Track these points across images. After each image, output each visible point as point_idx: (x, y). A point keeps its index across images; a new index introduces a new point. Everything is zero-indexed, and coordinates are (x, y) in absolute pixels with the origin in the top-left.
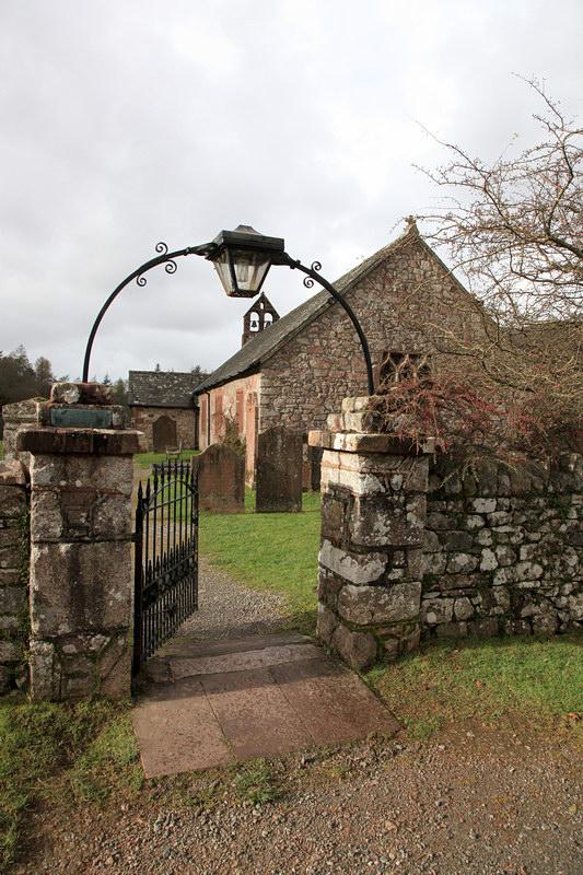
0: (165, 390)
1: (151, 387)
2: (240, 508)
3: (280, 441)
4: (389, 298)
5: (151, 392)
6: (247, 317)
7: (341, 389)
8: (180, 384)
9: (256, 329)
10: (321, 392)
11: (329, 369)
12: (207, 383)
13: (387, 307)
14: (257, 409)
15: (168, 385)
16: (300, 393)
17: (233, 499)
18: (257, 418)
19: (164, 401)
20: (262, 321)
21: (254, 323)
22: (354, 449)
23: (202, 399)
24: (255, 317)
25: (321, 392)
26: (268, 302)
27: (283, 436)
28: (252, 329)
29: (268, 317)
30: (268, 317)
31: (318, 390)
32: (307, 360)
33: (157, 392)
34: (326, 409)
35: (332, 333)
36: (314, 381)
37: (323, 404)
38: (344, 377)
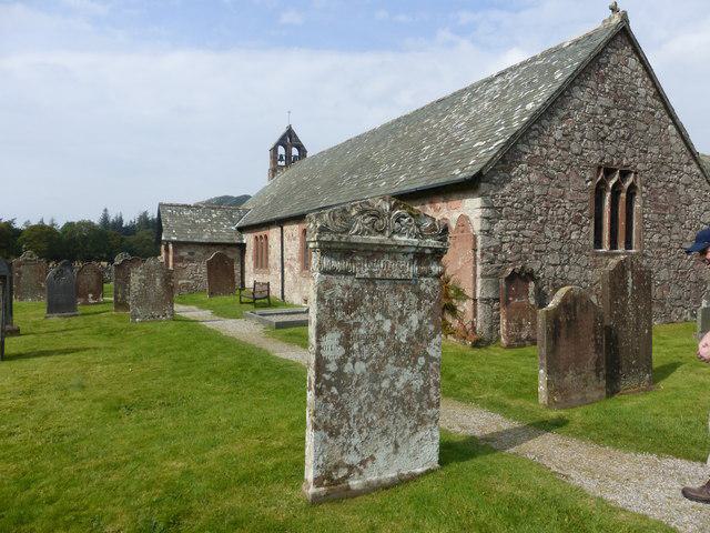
0: (205, 226)
3: (630, 281)
6: (275, 150)
9: (283, 163)
15: (206, 219)
17: (594, 377)
24: (281, 150)
30: (295, 152)
33: (194, 226)
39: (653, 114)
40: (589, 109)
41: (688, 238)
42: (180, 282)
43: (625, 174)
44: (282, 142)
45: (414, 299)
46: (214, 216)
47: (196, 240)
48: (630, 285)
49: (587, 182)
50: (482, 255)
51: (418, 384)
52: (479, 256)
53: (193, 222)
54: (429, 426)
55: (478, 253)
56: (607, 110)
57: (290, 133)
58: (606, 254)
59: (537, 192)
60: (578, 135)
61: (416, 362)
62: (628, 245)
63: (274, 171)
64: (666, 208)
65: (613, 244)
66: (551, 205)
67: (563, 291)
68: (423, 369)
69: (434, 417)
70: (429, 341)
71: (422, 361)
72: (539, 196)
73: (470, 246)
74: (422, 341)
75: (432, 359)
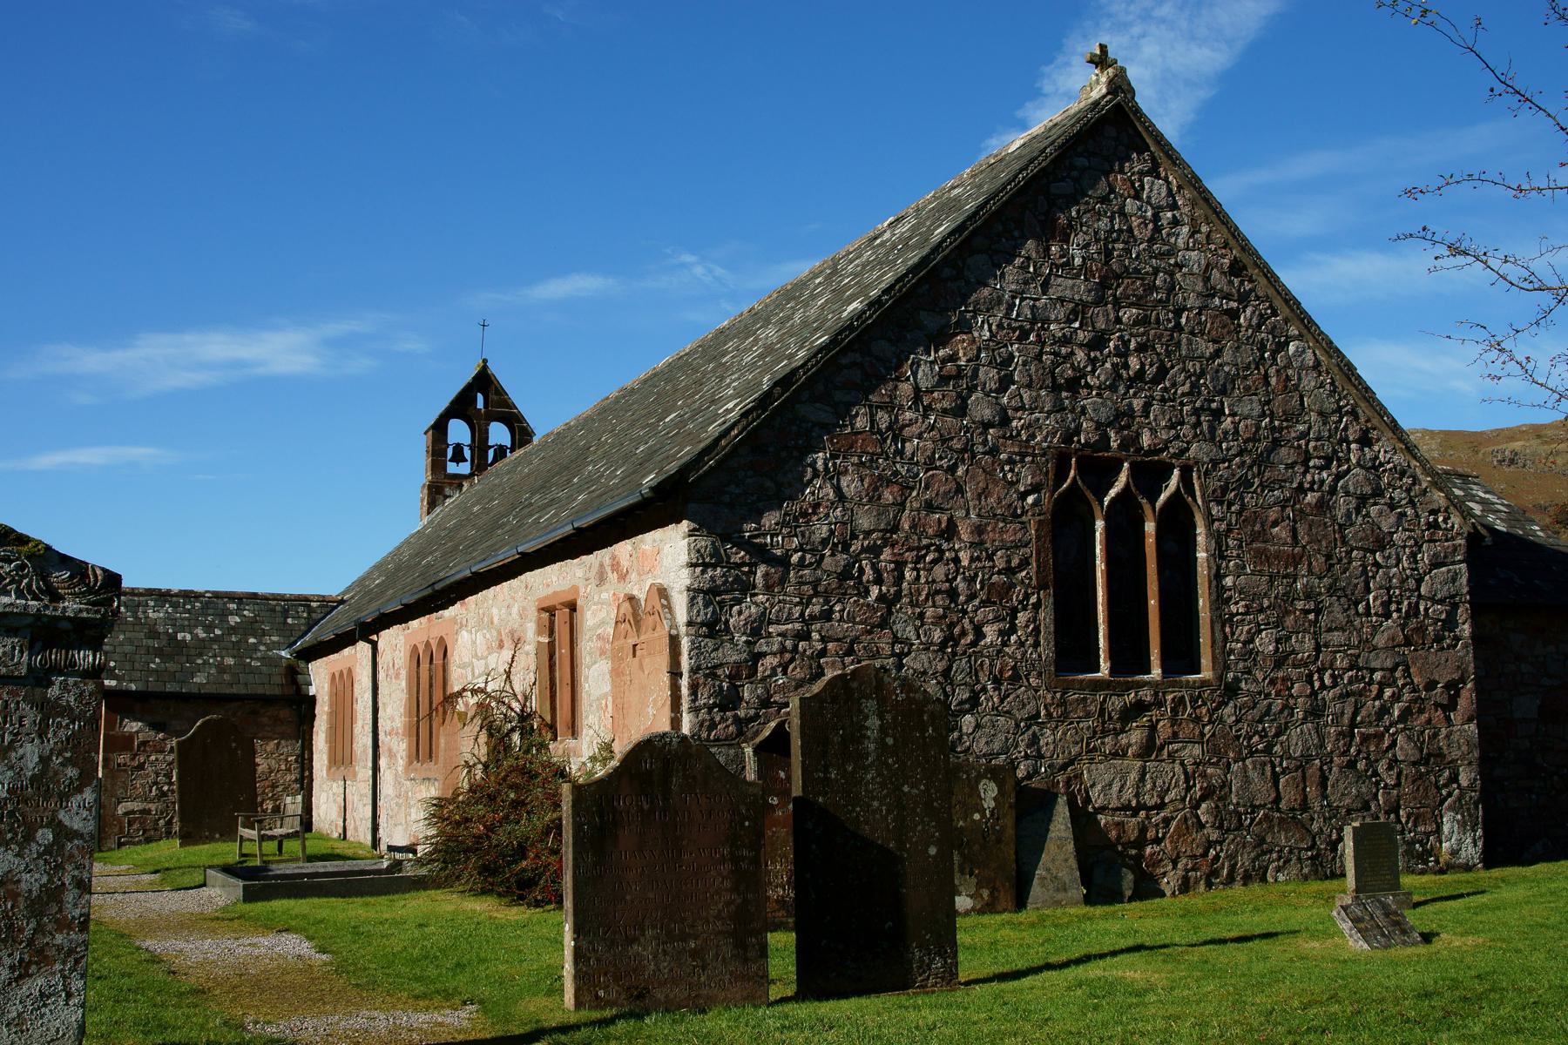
0: (201, 646)
1: (153, 634)
2: (753, 986)
3: (874, 722)
4: (1063, 286)
5: (159, 652)
6: (439, 429)
7: (939, 571)
8: (249, 627)
9: (464, 468)
10: (879, 581)
11: (901, 506)
12: (324, 631)
13: (1060, 312)
14: (674, 642)
15: (209, 628)
16: (815, 584)
17: (727, 950)
18: (675, 674)
19: (200, 679)
20: (480, 441)
21: (458, 449)
22: (790, 991)
23: (320, 676)
24: (459, 432)
25: (879, 581)
26: (500, 392)
27: (882, 701)
28: (452, 468)
29: (499, 434)
30: (499, 434)
31: (869, 574)
32: (833, 476)
33: (174, 649)
34: (896, 640)
35: (905, 389)
36: (856, 546)
37: (884, 623)
38: (950, 532)
39: (1234, 314)
40: (1022, 309)
41: (1380, 640)
42: (120, 810)
43: (1150, 474)
44: (460, 407)
45: (31, 716)
46: (234, 620)
47: (170, 688)
48: (873, 733)
49: (1023, 496)
50: (694, 688)
51: (32, 882)
52: (685, 691)
53: (173, 637)
54: (58, 967)
55: (684, 682)
56: (1078, 311)
57: (484, 381)
58: (1098, 685)
59: (864, 522)
60: (989, 376)
61: (29, 837)
62: (1181, 657)
63: (436, 493)
64: (1295, 560)
65: (1129, 657)
66: (909, 556)
67: (1348, 832)
68: (48, 850)
69: (71, 951)
70: (64, 797)
71: (45, 836)
72: (868, 534)
73: (663, 661)
74: (47, 795)
75: (74, 834)
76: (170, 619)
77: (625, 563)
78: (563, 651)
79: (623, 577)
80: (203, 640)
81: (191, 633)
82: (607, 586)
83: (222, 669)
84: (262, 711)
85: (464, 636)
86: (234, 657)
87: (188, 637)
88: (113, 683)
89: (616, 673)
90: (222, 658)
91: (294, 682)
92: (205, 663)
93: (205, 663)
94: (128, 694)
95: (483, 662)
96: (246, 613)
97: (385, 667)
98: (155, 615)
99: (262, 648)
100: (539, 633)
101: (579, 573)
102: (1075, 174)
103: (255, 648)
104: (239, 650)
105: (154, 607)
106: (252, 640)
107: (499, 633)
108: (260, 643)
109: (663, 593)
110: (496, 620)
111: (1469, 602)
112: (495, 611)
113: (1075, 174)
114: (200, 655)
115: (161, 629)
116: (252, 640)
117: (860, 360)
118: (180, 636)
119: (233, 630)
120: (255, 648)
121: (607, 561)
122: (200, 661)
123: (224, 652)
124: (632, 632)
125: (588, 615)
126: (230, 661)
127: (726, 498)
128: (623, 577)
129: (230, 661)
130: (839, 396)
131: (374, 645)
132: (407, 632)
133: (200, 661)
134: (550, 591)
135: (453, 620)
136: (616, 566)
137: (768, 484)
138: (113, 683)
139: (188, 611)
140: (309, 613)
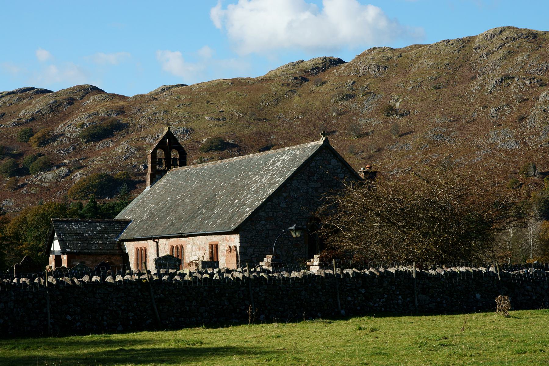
0: (92, 237)
1: (77, 234)
5: (80, 240)
15: (92, 232)
33: (83, 239)
46: (99, 228)
47: (85, 251)
76: (80, 229)
77: (228, 239)
78: (214, 253)
79: (228, 242)
80: (91, 236)
81: (87, 233)
82: (224, 243)
83: (99, 245)
84: (112, 258)
85: (189, 246)
86: (102, 241)
87: (87, 235)
88: (69, 250)
89: (226, 260)
90: (98, 241)
91: (121, 249)
92: (94, 243)
93: (94, 243)
94: (74, 253)
95: (195, 253)
96: (102, 226)
97: (161, 249)
98: (75, 228)
99: (109, 238)
100: (210, 249)
101: (219, 239)
102: (316, 161)
103: (107, 238)
104: (102, 238)
105: (75, 225)
106: (106, 235)
107: (199, 247)
108: (108, 236)
109: (235, 247)
110: (198, 244)
111: (249, 277)
112: (198, 242)
113: (316, 161)
114: (92, 241)
115: (78, 232)
116: (106, 235)
117: (271, 203)
118: (84, 234)
119: (99, 232)
120: (107, 238)
121: (224, 238)
122: (92, 243)
123: (98, 239)
124: (230, 253)
125: (221, 247)
126: (100, 242)
127: (246, 230)
128: (228, 242)
129: (100, 242)
130: (267, 210)
131: (157, 243)
132: (169, 241)
133: (92, 243)
134: (212, 241)
135: (186, 241)
136: (226, 239)
137: (254, 227)
138: (69, 250)
139: (85, 226)
140: (121, 226)
